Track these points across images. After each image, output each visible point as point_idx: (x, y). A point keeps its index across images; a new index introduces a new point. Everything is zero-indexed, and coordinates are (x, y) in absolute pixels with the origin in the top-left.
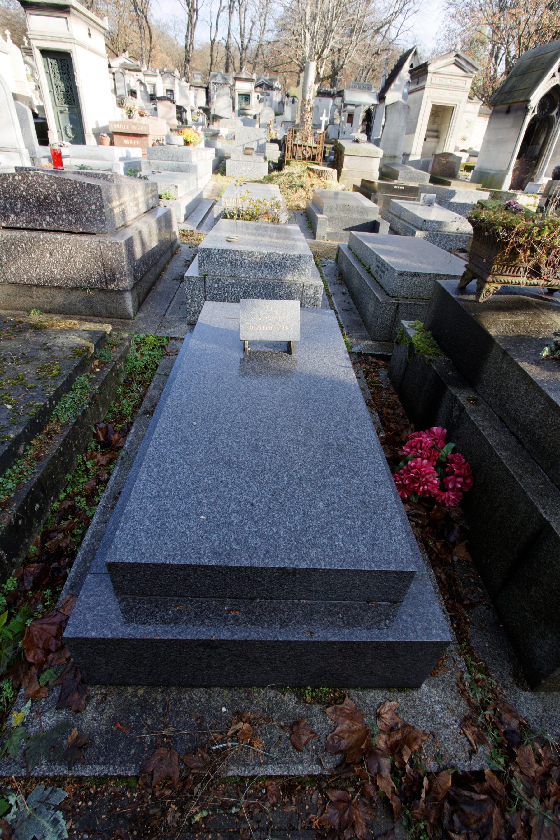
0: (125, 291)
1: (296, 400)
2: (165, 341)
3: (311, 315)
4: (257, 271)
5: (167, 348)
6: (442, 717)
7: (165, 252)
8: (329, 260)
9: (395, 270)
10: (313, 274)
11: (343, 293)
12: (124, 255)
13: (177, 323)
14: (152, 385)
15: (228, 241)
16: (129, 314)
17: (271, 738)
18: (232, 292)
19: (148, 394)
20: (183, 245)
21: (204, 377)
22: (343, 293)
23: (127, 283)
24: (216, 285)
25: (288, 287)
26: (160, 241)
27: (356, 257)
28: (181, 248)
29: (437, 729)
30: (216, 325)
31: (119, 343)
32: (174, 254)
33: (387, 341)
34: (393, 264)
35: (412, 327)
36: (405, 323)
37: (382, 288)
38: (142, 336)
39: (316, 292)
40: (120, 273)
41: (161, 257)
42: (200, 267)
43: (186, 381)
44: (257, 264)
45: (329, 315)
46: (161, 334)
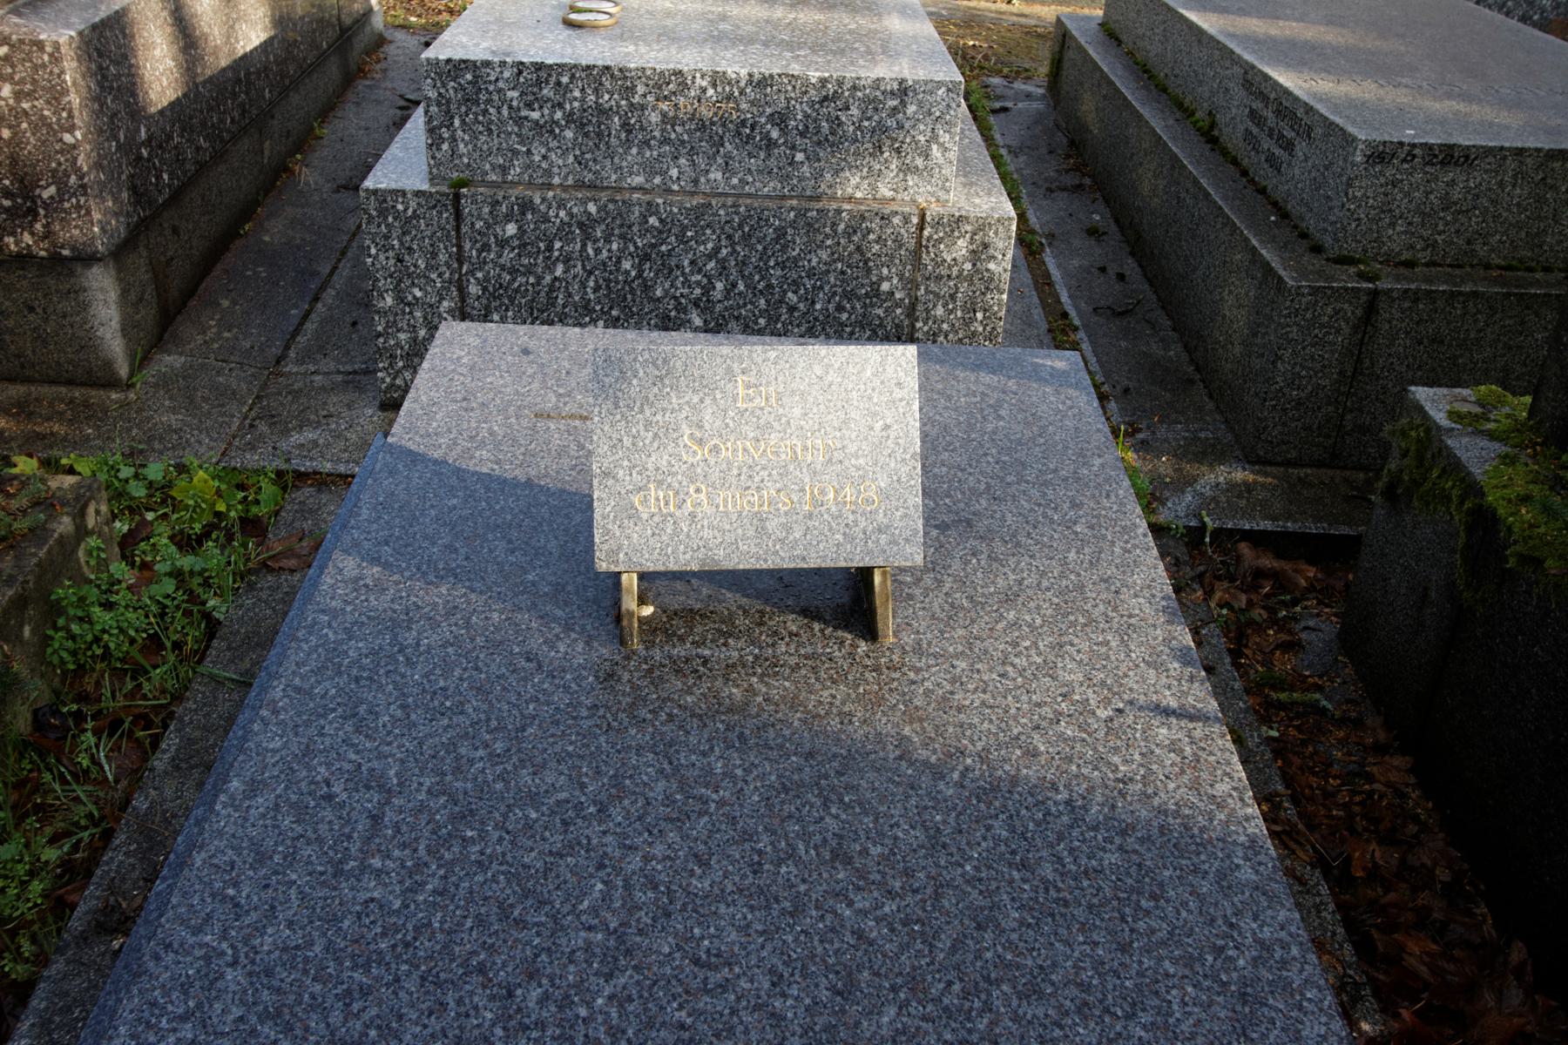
0: (86, 258)
1: (915, 983)
2: (268, 489)
3: (972, 385)
4: (701, 161)
5: (267, 536)
7: (307, 71)
8: (1019, 85)
9: (1349, 140)
10: (964, 164)
11: (1093, 232)
12: (74, 99)
13: (334, 401)
14: (171, 742)
15: (570, 24)
16: (108, 364)
18: (584, 258)
19: (140, 803)
20: (400, 35)
21: (376, 819)
22: (1093, 232)
23: (95, 222)
24: (511, 229)
25: (851, 231)
26: (281, 21)
27: (1144, 72)
28: (390, 50)
30: (483, 461)
31: (21, 525)
32: (351, 76)
33: (1320, 464)
34: (1336, 108)
35: (1470, 422)
36: (1434, 402)
37: (1284, 215)
38: (155, 471)
39: (980, 252)
40: (59, 180)
41: (284, 92)
42: (434, 145)
43: (262, 858)
44: (702, 126)
45: (1057, 377)
46: (252, 459)
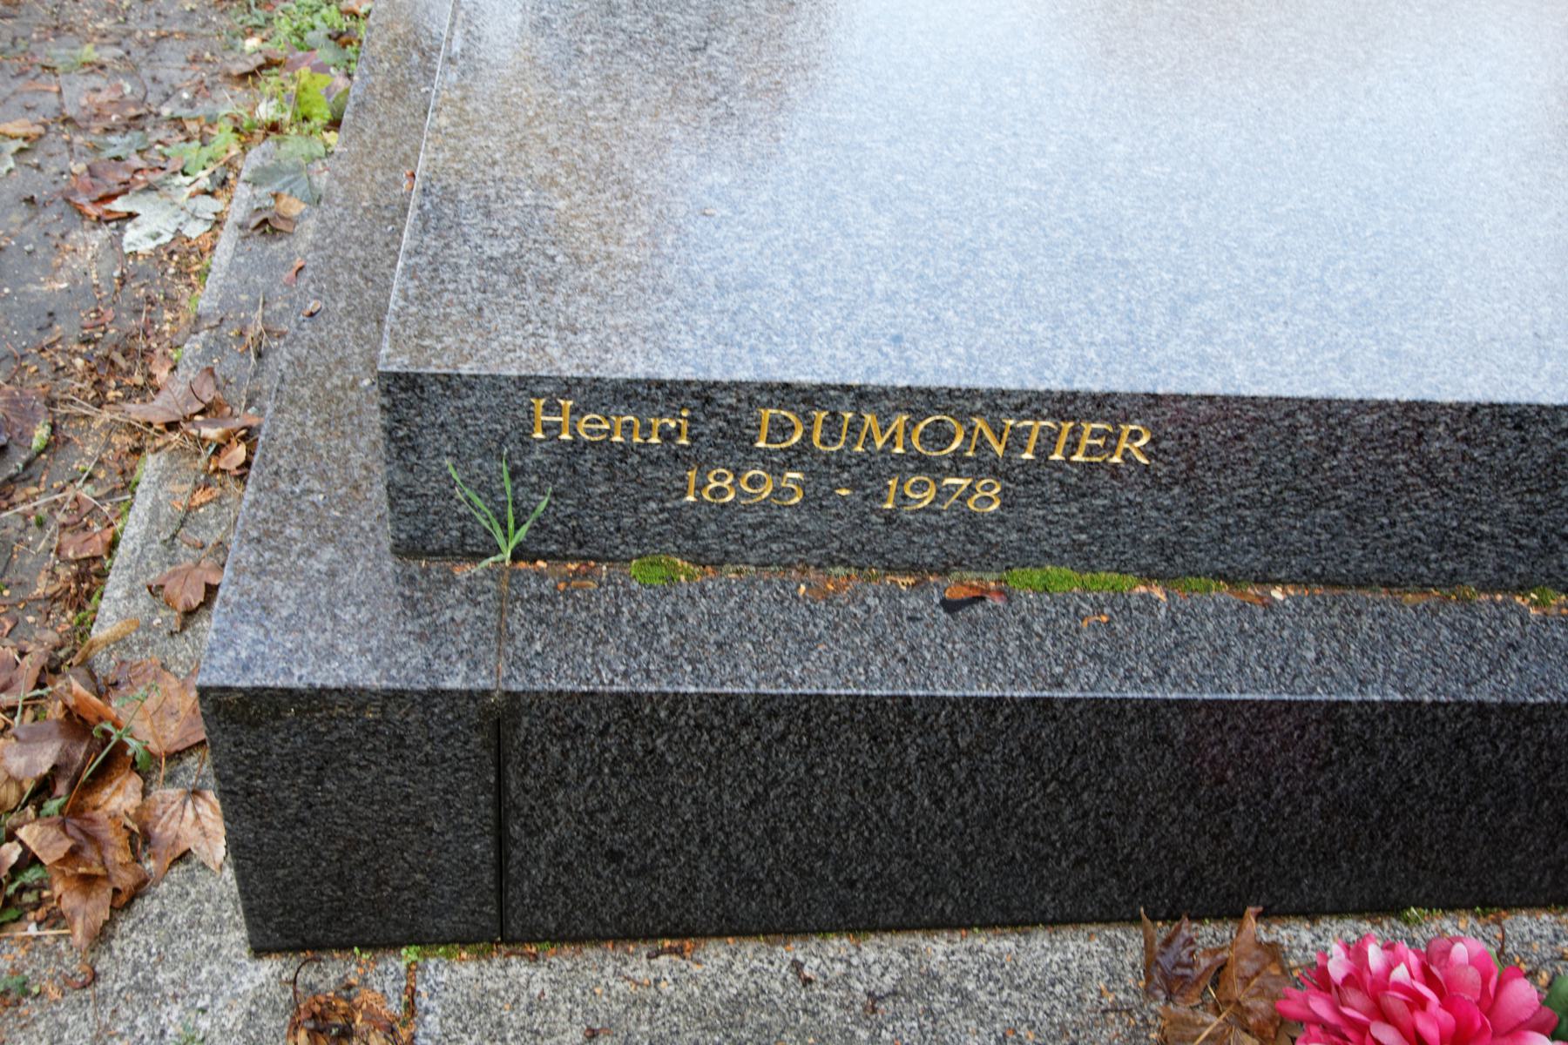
6: (133, 1028)
17: (206, 527)
29: (100, 1000)
